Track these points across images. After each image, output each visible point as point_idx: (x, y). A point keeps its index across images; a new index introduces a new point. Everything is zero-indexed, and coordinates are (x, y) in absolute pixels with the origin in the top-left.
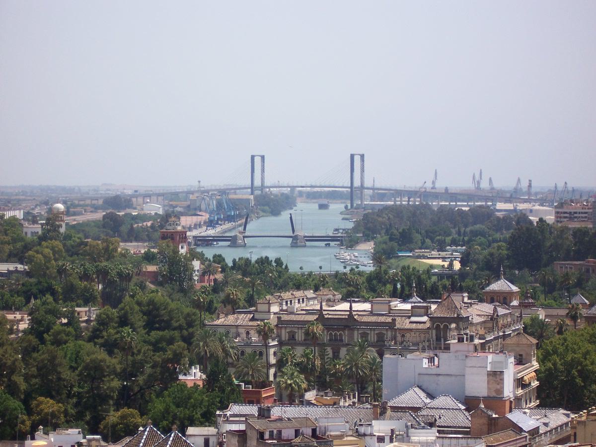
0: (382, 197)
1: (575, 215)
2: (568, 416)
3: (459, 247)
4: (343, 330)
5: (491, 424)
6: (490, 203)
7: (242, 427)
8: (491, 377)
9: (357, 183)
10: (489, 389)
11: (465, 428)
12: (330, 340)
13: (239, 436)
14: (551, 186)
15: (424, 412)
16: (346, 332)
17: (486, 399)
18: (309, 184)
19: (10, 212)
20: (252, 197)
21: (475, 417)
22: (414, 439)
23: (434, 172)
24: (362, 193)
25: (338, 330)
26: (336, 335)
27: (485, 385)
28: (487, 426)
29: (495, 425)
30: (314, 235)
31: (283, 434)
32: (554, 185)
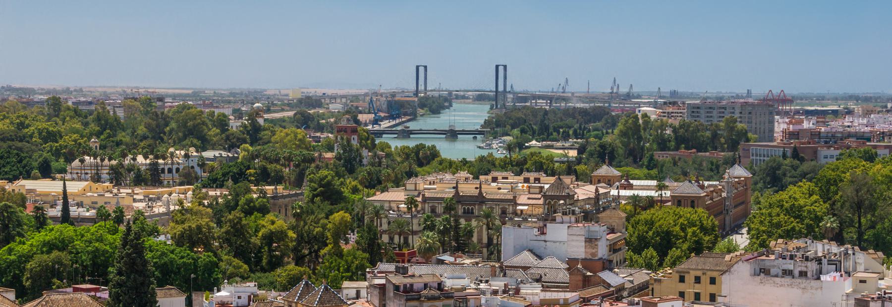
1: (672, 114)
2: (648, 274)
3: (579, 140)
5: (585, 281)
6: (606, 105)
7: (383, 281)
8: (587, 244)
9: (501, 88)
10: (586, 252)
11: (564, 283)
12: (464, 213)
13: (380, 288)
14: (743, 91)
15: (532, 271)
16: (477, 206)
17: (584, 260)
18: (462, 89)
19: (123, 111)
20: (416, 99)
21: (573, 275)
22: (822, 279)
23: (613, 79)
26: (468, 208)
27: (583, 250)
28: (582, 282)
29: (588, 282)
31: (414, 287)
32: (657, 90)
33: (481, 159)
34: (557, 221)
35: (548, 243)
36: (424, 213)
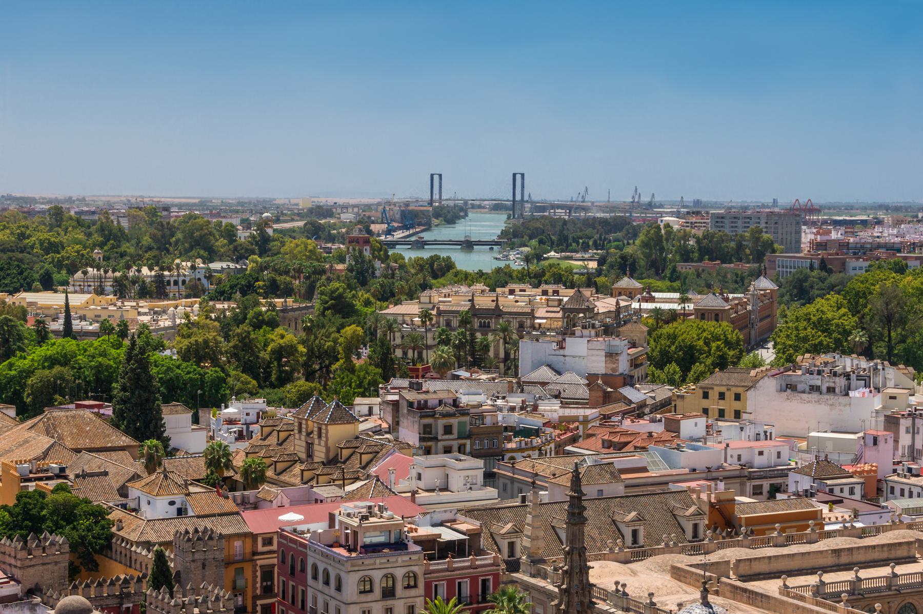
0: (543, 209)
2: (671, 390)
4: (491, 318)
7: (396, 398)
8: (607, 359)
9: (518, 198)
12: (480, 326)
13: (393, 405)
14: (769, 200)
15: (550, 387)
17: (604, 376)
20: (431, 209)
21: (593, 391)
22: (850, 395)
24: (522, 206)
25: (487, 318)
26: (485, 322)
27: (604, 365)
30: (438, 239)
32: (679, 199)
33: (498, 271)
34: (576, 335)
35: (567, 358)
36: (439, 327)
